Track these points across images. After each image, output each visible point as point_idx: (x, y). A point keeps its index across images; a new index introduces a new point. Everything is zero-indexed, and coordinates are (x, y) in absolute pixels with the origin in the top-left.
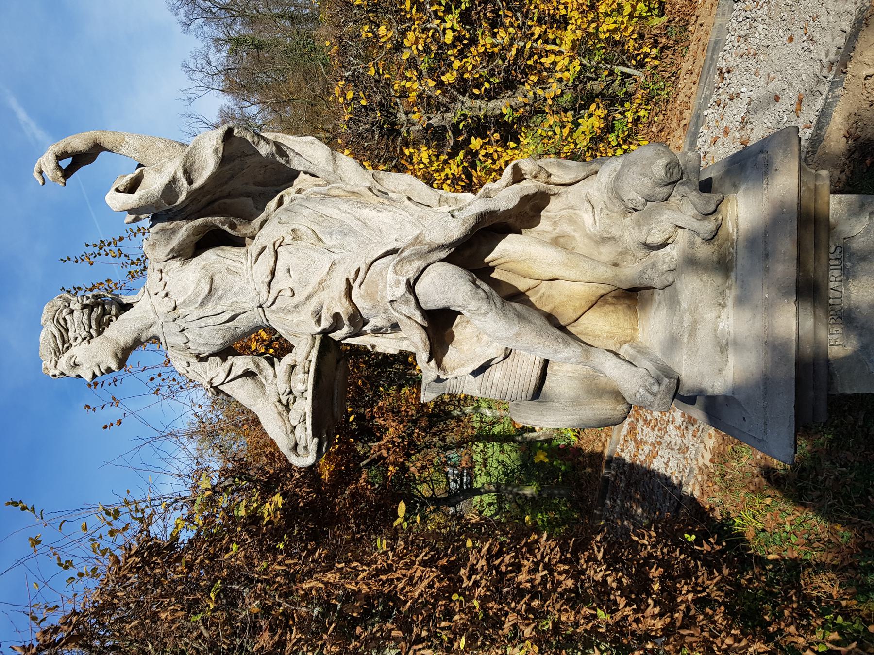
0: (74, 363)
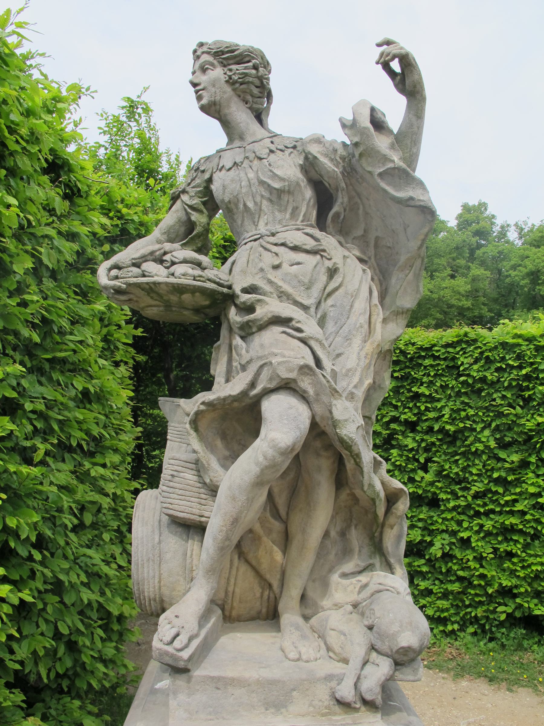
0: (207, 69)
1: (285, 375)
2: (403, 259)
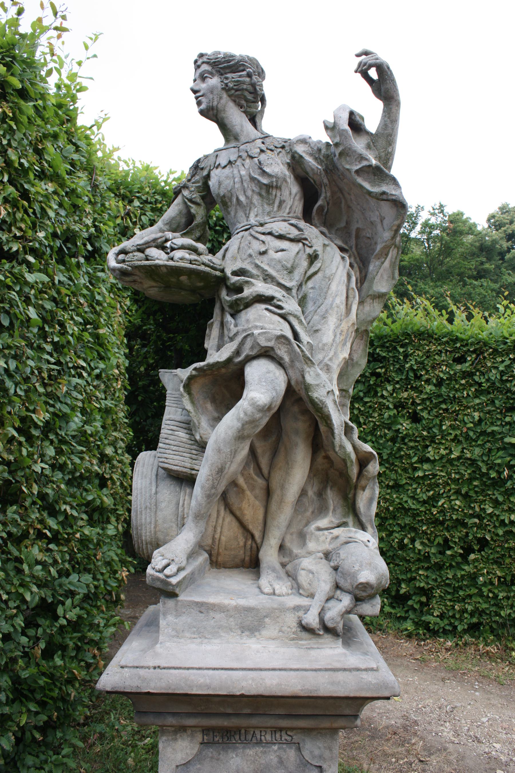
1: (263, 343)
2: (379, 247)
